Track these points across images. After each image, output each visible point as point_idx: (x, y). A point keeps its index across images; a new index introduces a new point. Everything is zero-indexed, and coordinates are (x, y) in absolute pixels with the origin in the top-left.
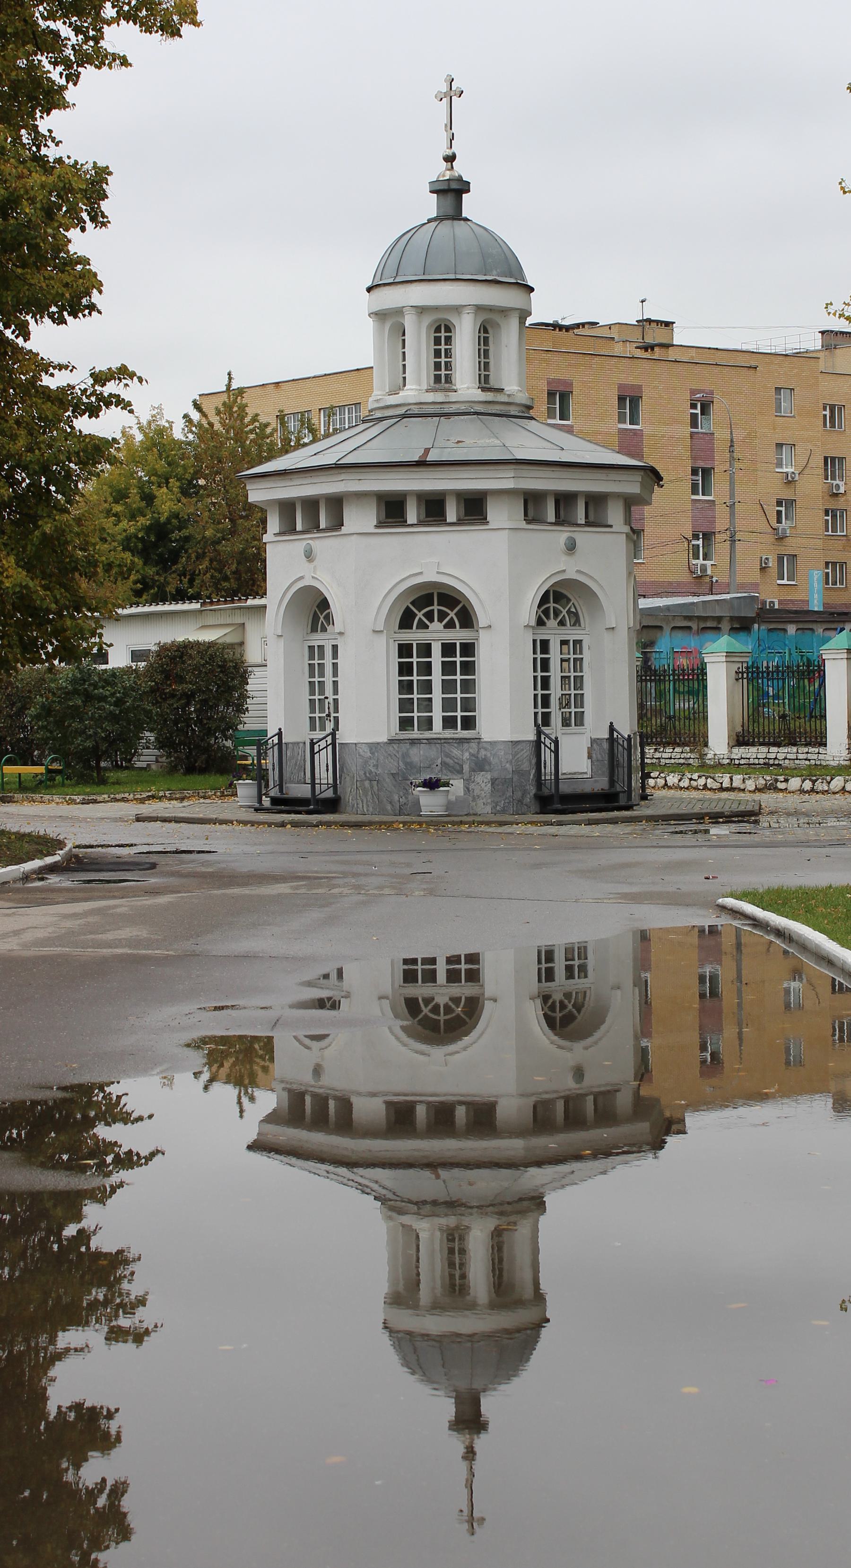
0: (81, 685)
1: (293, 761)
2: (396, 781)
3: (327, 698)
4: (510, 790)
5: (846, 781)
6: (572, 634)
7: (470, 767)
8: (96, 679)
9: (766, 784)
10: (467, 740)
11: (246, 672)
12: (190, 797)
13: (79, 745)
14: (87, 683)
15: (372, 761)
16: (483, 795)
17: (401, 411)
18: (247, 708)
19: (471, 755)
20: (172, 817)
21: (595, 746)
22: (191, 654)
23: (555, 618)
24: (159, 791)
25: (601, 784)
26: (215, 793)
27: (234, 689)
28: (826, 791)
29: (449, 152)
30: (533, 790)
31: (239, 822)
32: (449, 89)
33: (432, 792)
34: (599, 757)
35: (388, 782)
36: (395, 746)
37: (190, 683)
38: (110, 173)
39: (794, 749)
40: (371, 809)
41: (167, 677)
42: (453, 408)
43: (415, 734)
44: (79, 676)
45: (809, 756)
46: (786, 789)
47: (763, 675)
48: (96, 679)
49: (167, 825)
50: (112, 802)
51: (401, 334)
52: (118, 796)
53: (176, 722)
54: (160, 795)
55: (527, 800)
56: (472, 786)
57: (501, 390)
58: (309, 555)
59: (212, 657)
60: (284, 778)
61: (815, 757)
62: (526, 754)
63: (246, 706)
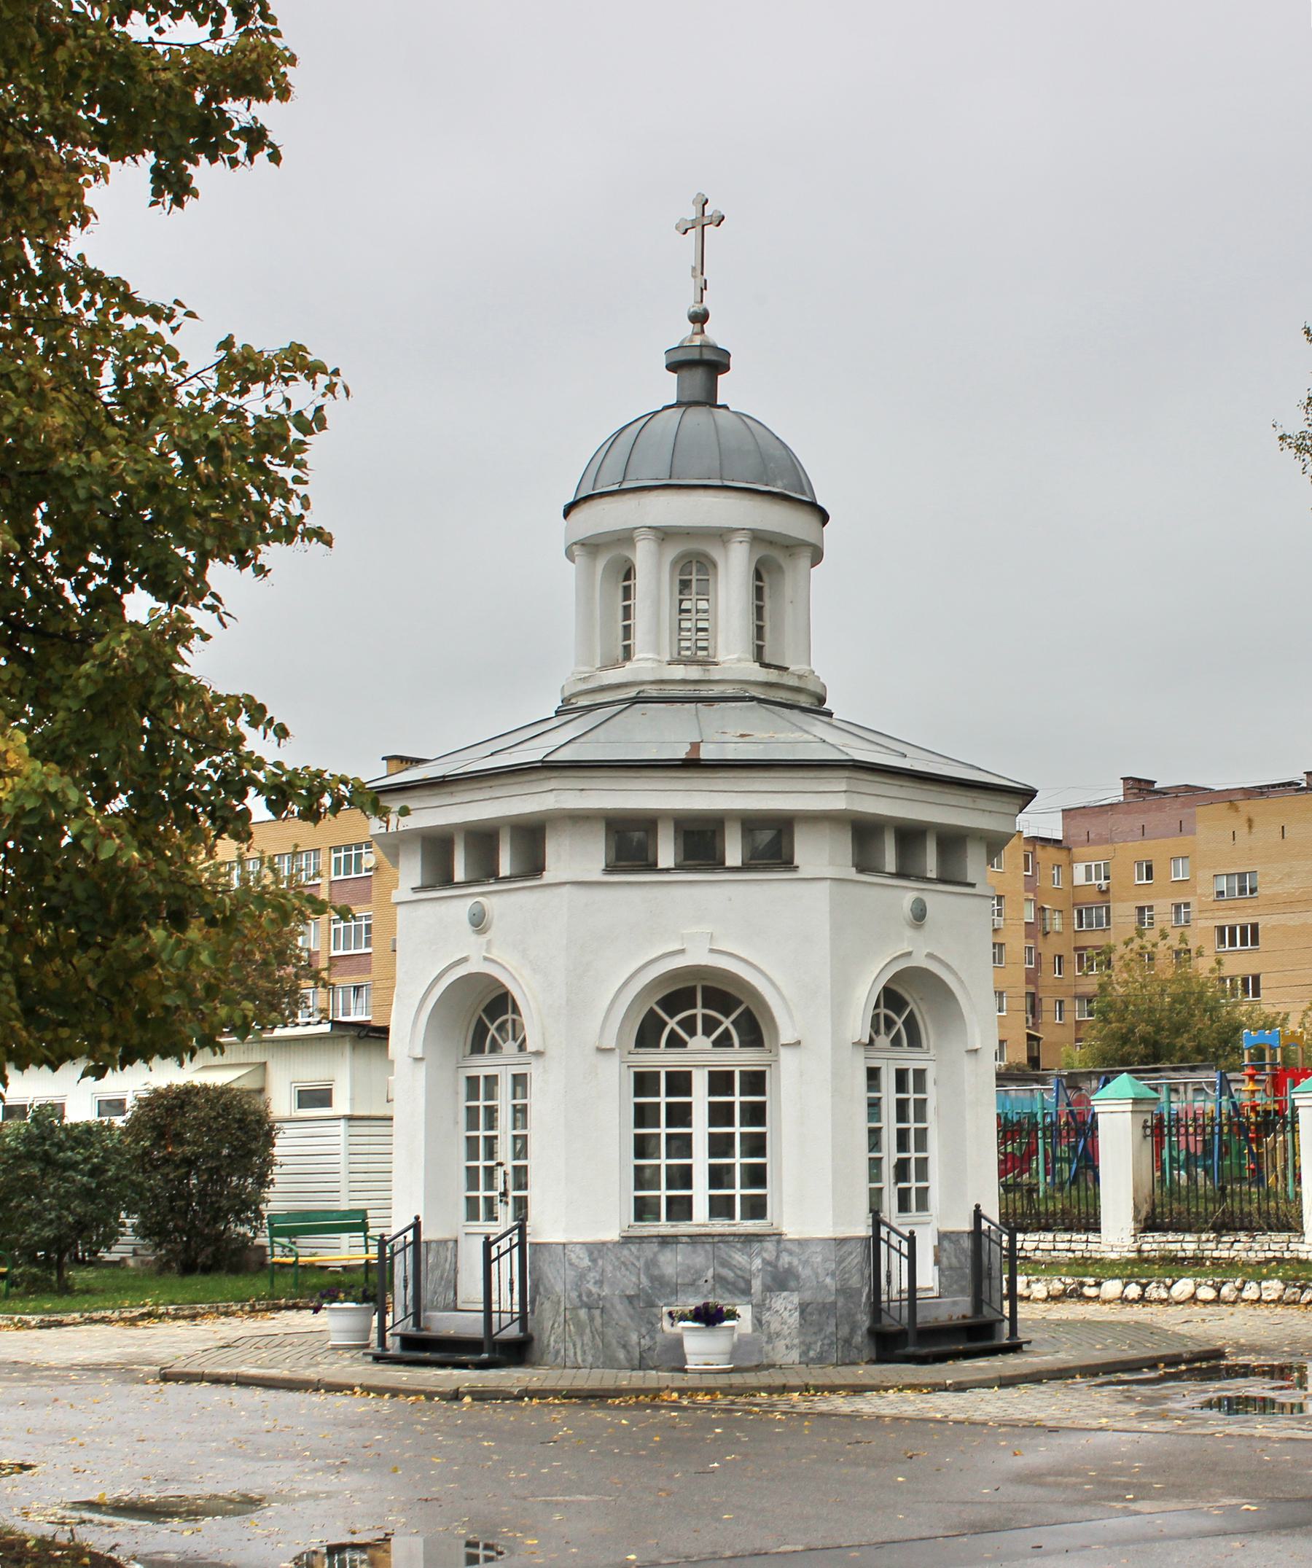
0: (39, 1145)
1: (438, 1273)
2: (634, 1308)
3: (500, 1164)
4: (833, 1321)
5: (1198, 1286)
6: (911, 1060)
7: (764, 1284)
8: (62, 1136)
9: (1065, 1290)
10: (749, 1239)
11: (272, 1128)
12: (204, 1314)
13: (34, 1235)
14: (48, 1142)
15: (592, 1275)
16: (786, 1332)
17: (632, 693)
18: (273, 1179)
19: (765, 1261)
20: (232, 1375)
21: (946, 1244)
22: (196, 1103)
23: (887, 1034)
24: (157, 1304)
25: (958, 1307)
26: (242, 1307)
27: (251, 1153)
28: (1165, 1300)
29: (698, 308)
30: (864, 1321)
31: (367, 1389)
32: (699, 215)
33: (710, 1328)
34: (954, 1262)
35: (620, 1310)
36: (634, 1248)
37: (195, 1143)
38: (178, 202)
39: (1050, 1236)
40: (590, 1359)
41: (161, 1136)
42: (716, 690)
43: (663, 1226)
44: (35, 1131)
45: (1074, 1246)
46: (1098, 1297)
47: (1187, 1131)
48: (62, 1136)
49: (222, 1389)
50: (86, 1324)
51: (621, 577)
52: (96, 1315)
53: (172, 1199)
54: (160, 1311)
55: (858, 1339)
56: (766, 1317)
57: (784, 669)
58: (479, 922)
59: (227, 1108)
60: (423, 1302)
61: (1083, 1246)
62: (856, 1261)
63: (271, 1177)
